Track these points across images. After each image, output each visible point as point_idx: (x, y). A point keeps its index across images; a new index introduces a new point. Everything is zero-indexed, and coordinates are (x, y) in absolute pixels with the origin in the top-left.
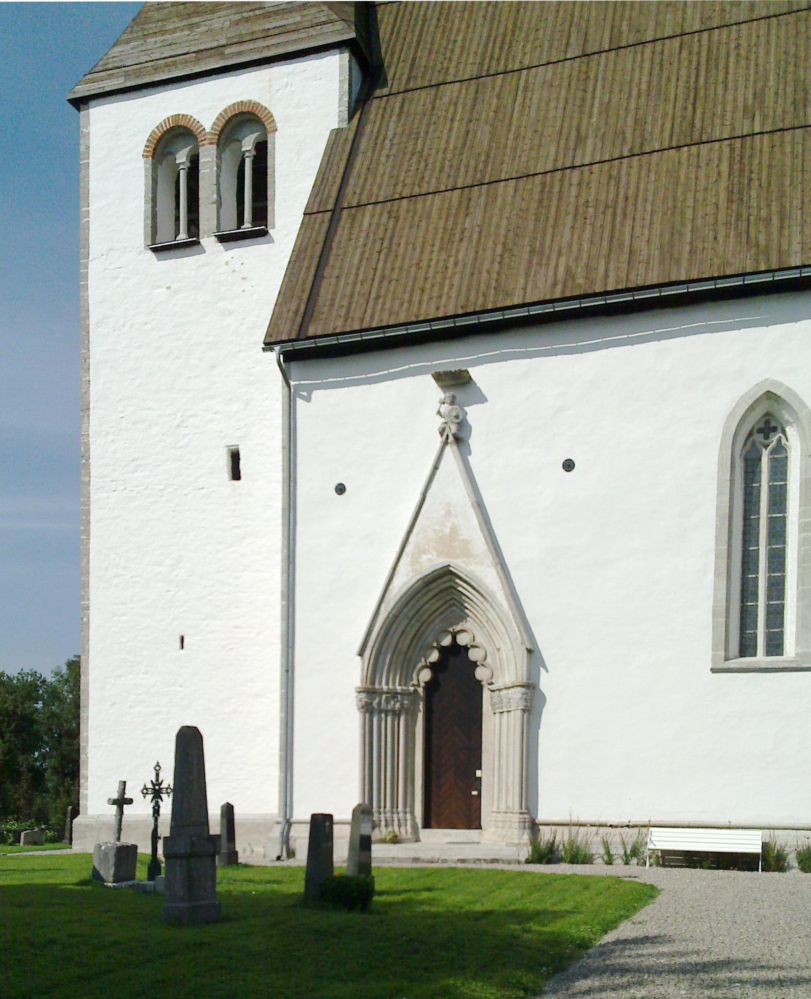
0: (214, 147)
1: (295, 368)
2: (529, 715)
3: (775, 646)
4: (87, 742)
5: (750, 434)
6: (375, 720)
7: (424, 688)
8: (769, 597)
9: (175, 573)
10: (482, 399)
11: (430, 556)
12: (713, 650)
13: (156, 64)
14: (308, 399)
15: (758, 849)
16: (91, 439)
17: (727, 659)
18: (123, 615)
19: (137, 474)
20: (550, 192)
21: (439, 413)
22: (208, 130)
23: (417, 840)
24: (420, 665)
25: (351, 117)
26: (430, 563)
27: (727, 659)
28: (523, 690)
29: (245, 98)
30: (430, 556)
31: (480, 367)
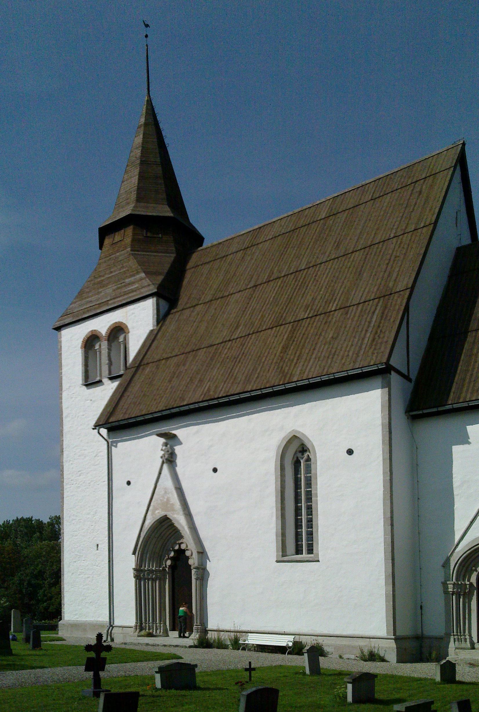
0: (106, 342)
2: (203, 581)
3: (310, 551)
7: (168, 568)
9: (94, 518)
10: (181, 443)
11: (158, 511)
12: (277, 552)
13: (88, 310)
14: (116, 447)
18: (76, 536)
19: (81, 477)
22: (104, 335)
23: (168, 636)
24: (166, 558)
26: (159, 513)
29: (117, 321)
30: (158, 511)
31: (179, 430)
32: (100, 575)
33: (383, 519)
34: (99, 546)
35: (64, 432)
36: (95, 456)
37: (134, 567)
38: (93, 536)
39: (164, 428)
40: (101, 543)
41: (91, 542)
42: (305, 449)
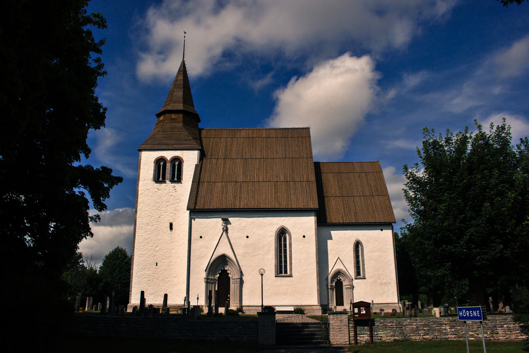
0: (170, 163)
1: (191, 213)
3: (286, 272)
4: (132, 286)
5: (280, 234)
6: (208, 285)
8: (284, 263)
9: (156, 249)
10: (231, 224)
15: (293, 310)
16: (137, 218)
17: (277, 274)
20: (242, 186)
21: (222, 225)
22: (169, 160)
25: (200, 162)
27: (277, 274)
28: (240, 279)
29: (177, 155)
32: (158, 279)
33: (316, 262)
34: (158, 264)
35: (138, 202)
36: (158, 217)
37: (205, 277)
38: (155, 259)
39: (225, 217)
40: (159, 262)
41: (153, 261)
42: (284, 232)
